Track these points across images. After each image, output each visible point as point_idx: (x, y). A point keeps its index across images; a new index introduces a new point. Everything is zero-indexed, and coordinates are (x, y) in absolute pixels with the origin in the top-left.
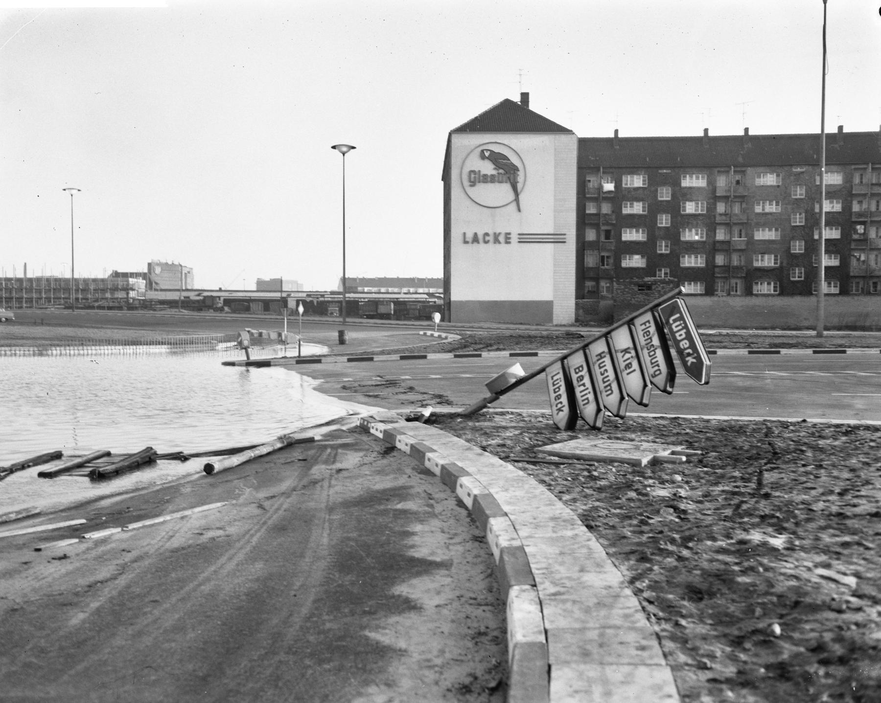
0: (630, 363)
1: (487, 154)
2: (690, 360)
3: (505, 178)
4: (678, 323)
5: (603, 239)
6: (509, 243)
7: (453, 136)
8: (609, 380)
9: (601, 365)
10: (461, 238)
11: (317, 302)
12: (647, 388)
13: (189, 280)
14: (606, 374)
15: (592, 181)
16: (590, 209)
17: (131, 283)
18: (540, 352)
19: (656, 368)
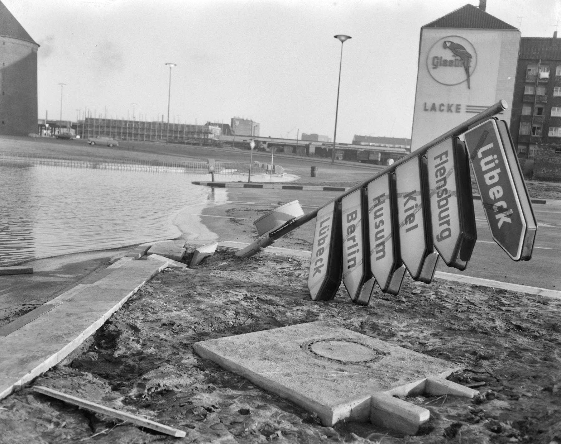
0: (413, 215)
1: (448, 44)
2: (502, 218)
3: (460, 63)
4: (490, 158)
5: (535, 114)
6: (459, 112)
7: (424, 30)
8: (383, 236)
9: (378, 214)
10: (422, 107)
11: (329, 149)
12: (430, 256)
13: (256, 131)
14: (381, 228)
15: (532, 70)
16: (528, 92)
17: (210, 129)
18: (546, 200)
19: (445, 226)
